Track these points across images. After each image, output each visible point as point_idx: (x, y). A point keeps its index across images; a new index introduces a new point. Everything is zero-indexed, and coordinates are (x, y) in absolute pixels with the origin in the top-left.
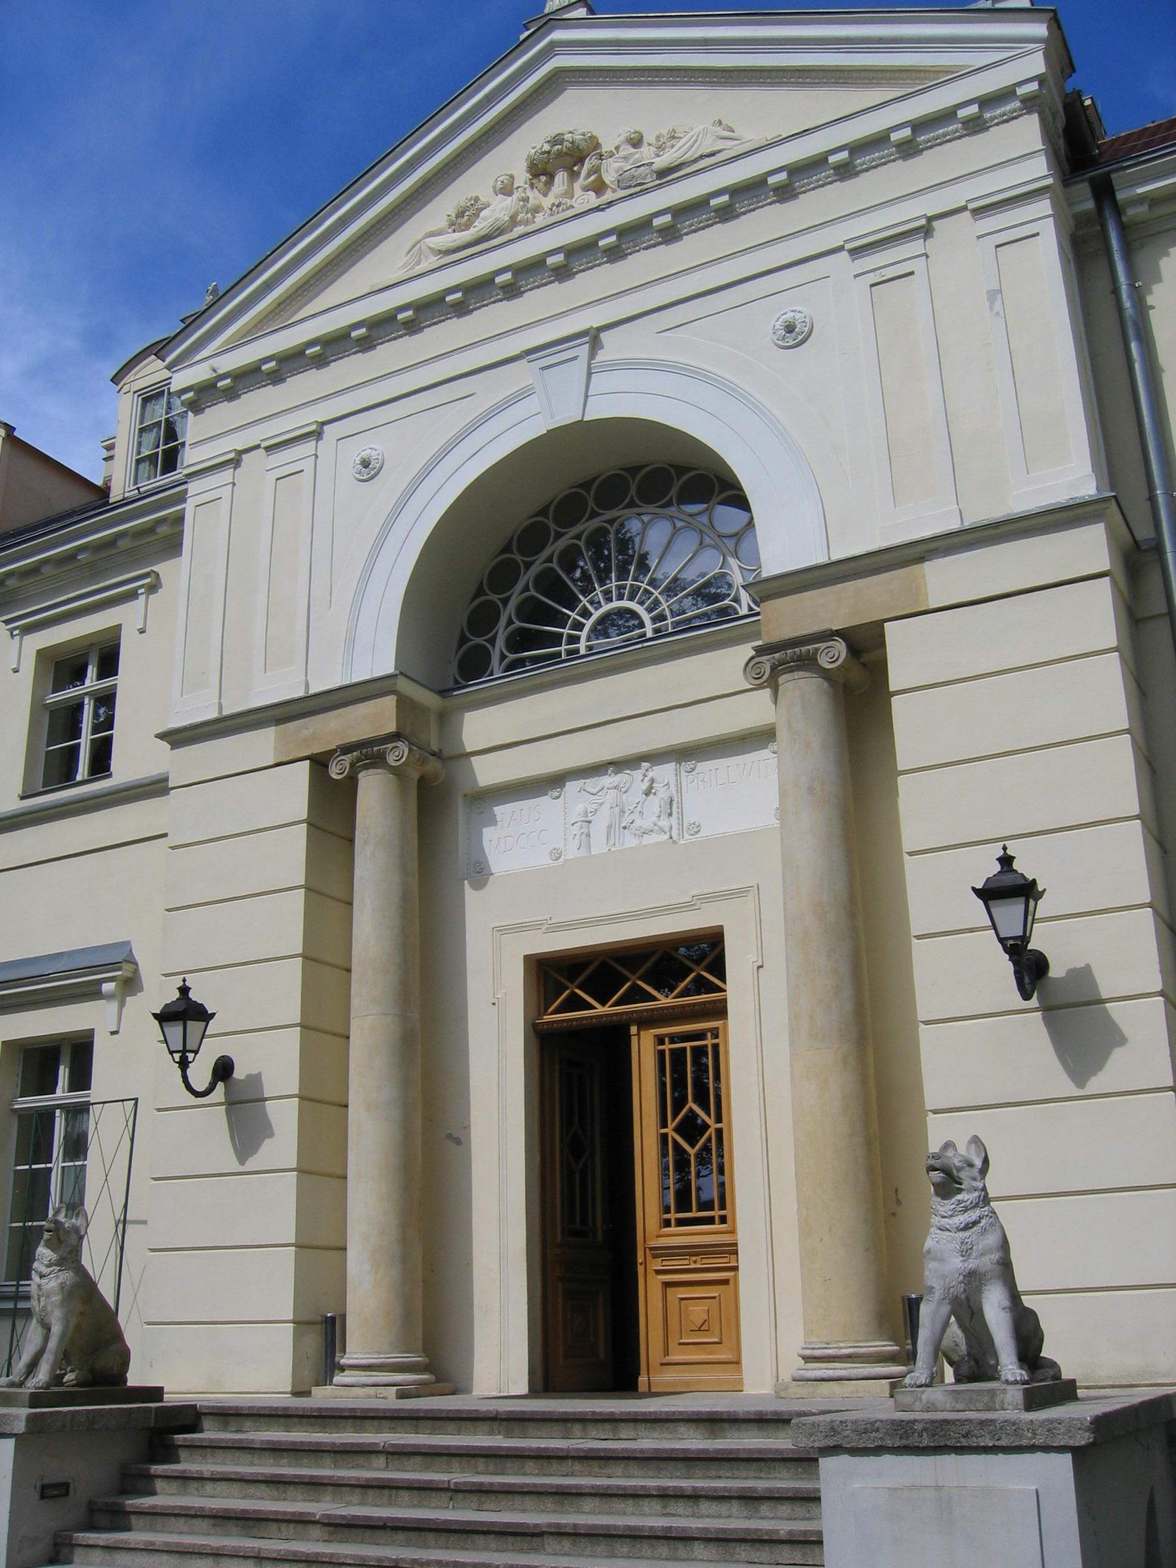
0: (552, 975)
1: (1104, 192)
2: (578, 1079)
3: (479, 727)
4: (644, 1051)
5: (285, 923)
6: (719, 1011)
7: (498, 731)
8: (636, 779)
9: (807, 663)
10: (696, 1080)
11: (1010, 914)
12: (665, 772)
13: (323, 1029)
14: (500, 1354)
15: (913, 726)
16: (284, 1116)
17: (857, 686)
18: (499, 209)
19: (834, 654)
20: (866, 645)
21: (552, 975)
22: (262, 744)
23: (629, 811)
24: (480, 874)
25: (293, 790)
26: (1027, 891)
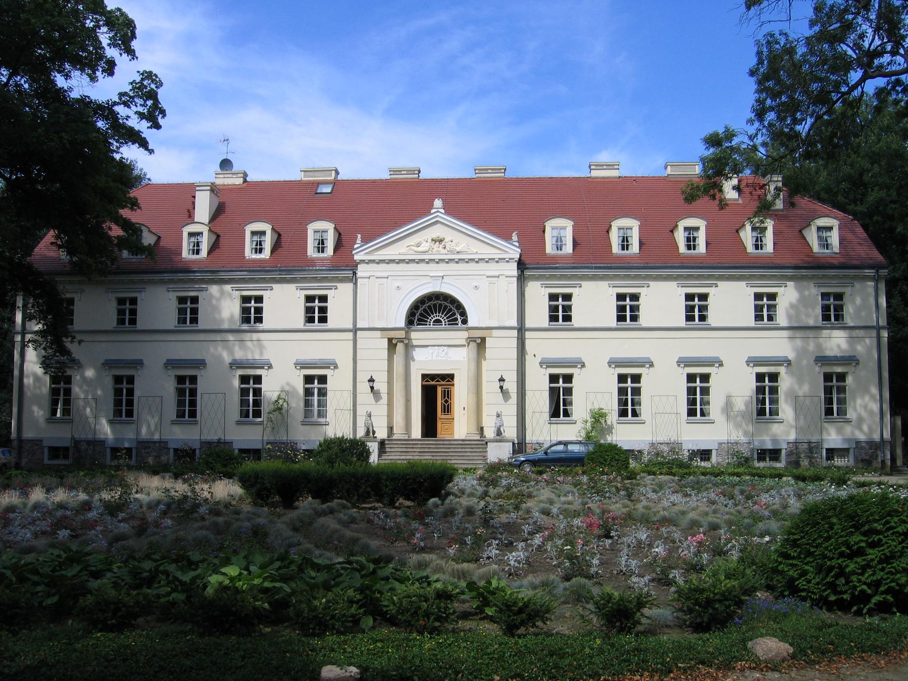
0: (424, 377)
1: (522, 272)
2: (429, 394)
3: (414, 335)
4: (439, 389)
5: (384, 365)
6: (453, 385)
7: (418, 336)
8: (441, 348)
9: (475, 341)
10: (447, 395)
11: (502, 383)
12: (446, 348)
13: (390, 382)
14: (416, 432)
15: (489, 353)
16: (385, 397)
17: (481, 344)
18: (424, 247)
19: (479, 341)
20: (483, 340)
21: (424, 377)
22: (378, 333)
23: (438, 351)
24: (414, 360)
25: (385, 343)
26: (504, 380)
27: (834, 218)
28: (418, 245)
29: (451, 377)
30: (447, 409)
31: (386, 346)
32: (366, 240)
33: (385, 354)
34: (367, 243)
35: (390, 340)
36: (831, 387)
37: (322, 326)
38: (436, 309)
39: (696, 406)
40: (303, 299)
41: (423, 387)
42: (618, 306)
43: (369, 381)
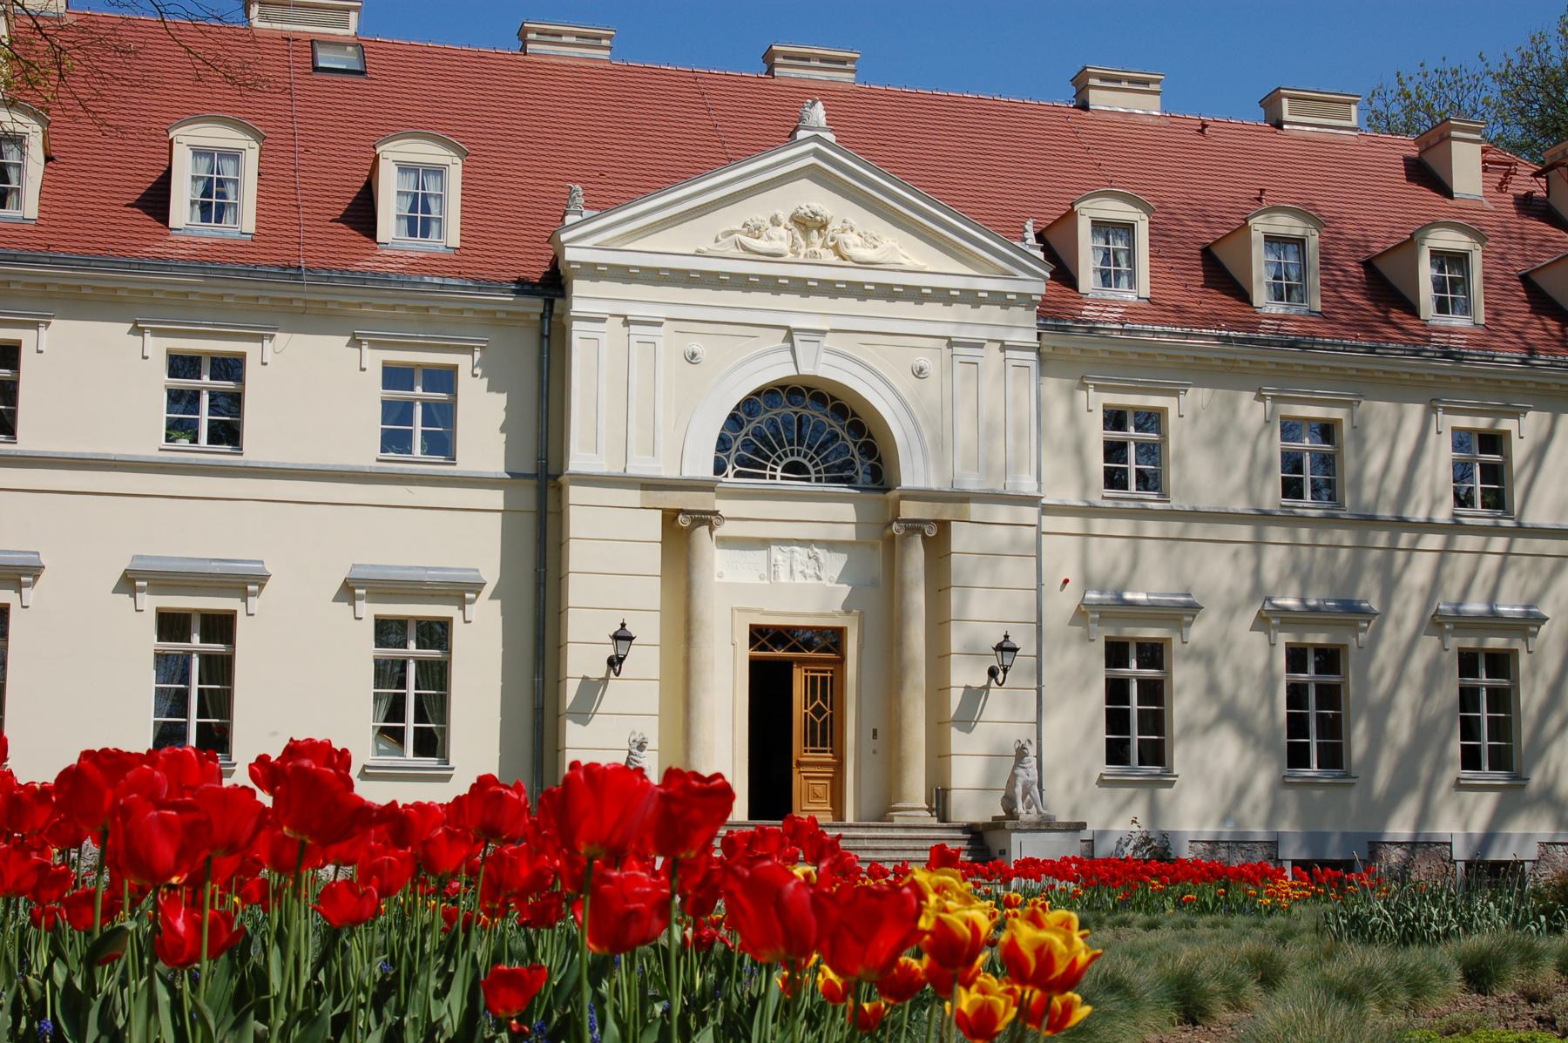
0: (760, 636)
10: (828, 690)
20: (944, 526)
21: (760, 636)
22: (634, 496)
27: (35, 116)
28: (755, 231)
29: (751, 626)
30: (827, 733)
31: (657, 533)
32: (603, 205)
33: (652, 557)
34: (605, 210)
35: (670, 517)
36: (1475, 691)
37: (222, 455)
38: (807, 433)
39: (1137, 733)
40: (377, 375)
41: (755, 666)
42: (387, 405)
43: (616, 637)
